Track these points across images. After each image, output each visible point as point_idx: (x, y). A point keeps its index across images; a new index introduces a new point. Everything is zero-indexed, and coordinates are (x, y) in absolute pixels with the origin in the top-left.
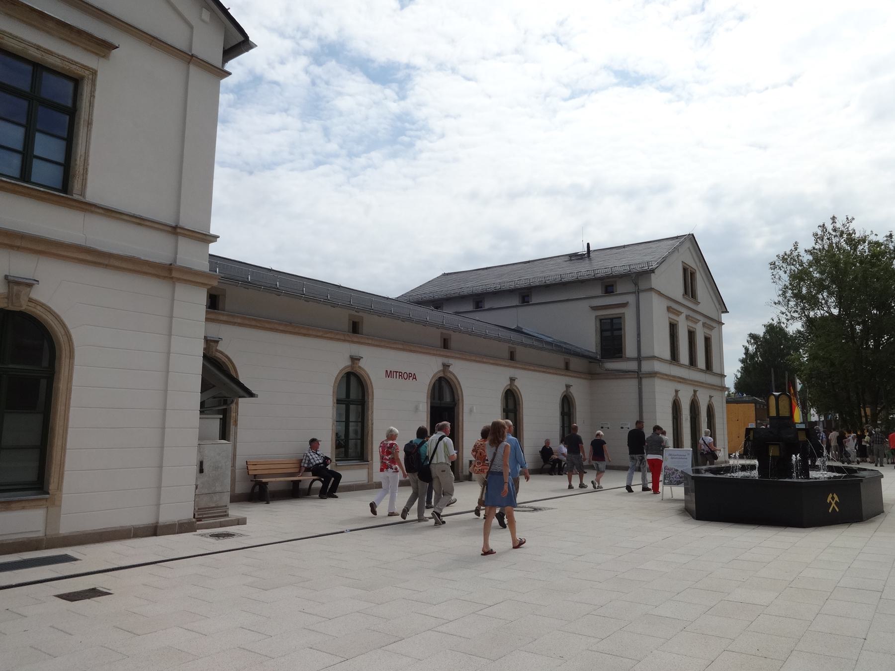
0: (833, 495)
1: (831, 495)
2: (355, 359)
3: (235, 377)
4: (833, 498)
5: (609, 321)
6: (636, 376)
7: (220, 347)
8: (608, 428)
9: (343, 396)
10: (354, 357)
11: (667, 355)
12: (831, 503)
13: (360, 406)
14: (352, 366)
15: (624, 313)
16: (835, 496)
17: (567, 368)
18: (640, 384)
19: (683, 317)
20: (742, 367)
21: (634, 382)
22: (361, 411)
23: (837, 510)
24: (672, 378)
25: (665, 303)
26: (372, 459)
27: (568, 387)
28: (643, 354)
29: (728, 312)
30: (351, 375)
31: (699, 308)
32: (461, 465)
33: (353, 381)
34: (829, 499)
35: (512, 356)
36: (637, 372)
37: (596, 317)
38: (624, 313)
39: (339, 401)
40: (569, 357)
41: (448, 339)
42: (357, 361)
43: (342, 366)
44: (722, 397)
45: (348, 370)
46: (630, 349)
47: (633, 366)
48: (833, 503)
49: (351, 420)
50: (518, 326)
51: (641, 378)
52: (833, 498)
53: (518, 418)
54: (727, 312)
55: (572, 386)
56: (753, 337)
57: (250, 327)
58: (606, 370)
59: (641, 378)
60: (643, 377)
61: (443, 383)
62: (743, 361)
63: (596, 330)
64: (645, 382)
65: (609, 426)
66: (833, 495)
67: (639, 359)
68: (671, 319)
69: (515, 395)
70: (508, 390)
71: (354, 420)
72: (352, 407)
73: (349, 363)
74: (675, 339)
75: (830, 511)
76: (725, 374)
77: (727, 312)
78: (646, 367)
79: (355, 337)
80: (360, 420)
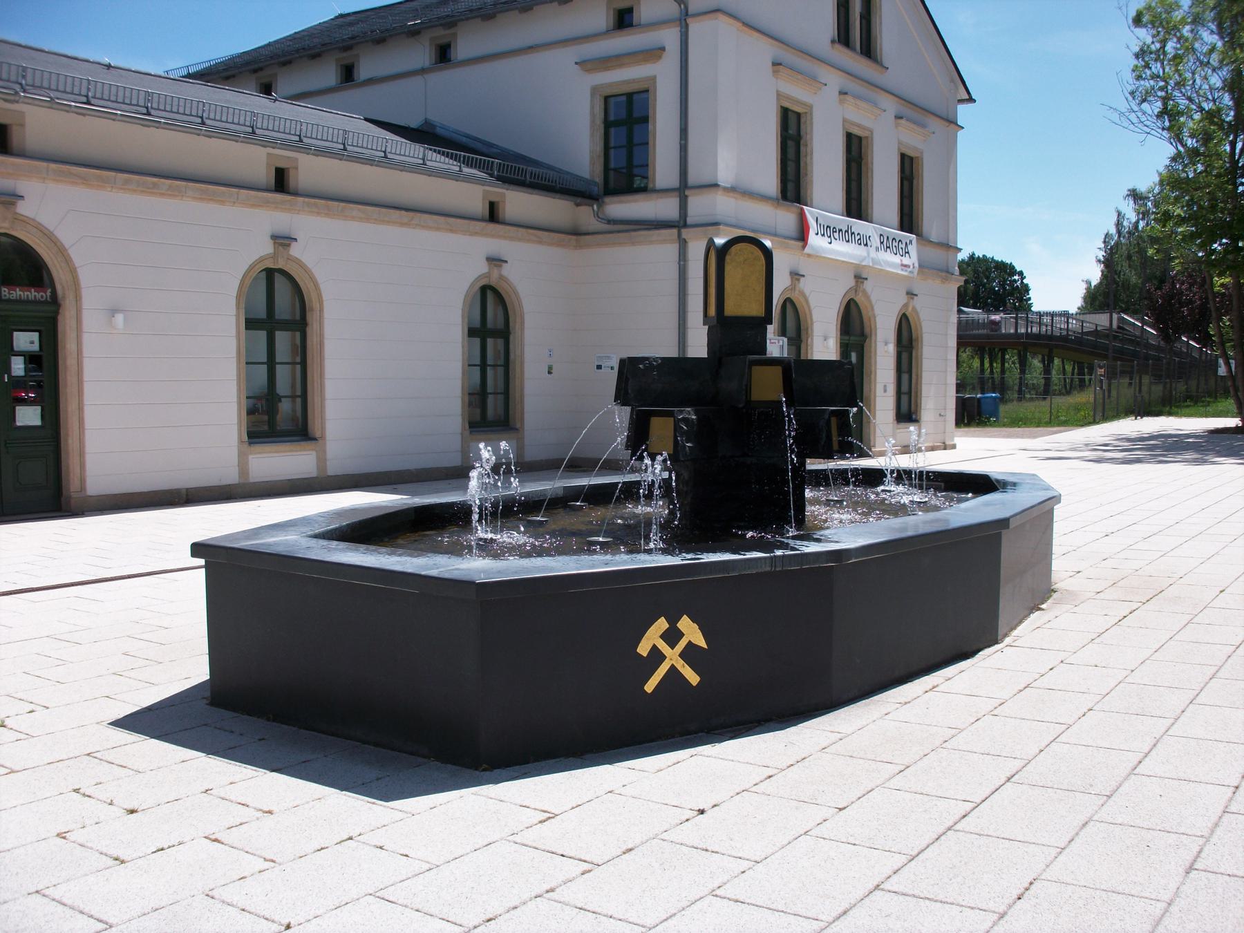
0: (673, 621)
1: (662, 624)
2: (282, 241)
3: (296, 296)
4: (672, 636)
5: (624, 98)
11: (769, 181)
12: (656, 656)
13: (298, 334)
15: (653, 79)
16: (685, 624)
17: (493, 214)
19: (831, 92)
23: (650, 687)
25: (764, 51)
27: (495, 261)
28: (693, 178)
29: (975, 101)
30: (276, 274)
31: (887, 79)
32: (78, 470)
34: (652, 638)
35: (281, 182)
37: (594, 90)
38: (653, 79)
40: (504, 191)
41: (10, 125)
46: (664, 169)
47: (666, 208)
48: (672, 657)
52: (672, 636)
54: (971, 100)
56: (1135, 195)
61: (788, 305)
63: (593, 122)
66: (673, 621)
67: (683, 189)
68: (788, 98)
70: (484, 290)
71: (492, 364)
73: (267, 248)
74: (802, 148)
77: (971, 100)
78: (698, 206)
80: (298, 359)
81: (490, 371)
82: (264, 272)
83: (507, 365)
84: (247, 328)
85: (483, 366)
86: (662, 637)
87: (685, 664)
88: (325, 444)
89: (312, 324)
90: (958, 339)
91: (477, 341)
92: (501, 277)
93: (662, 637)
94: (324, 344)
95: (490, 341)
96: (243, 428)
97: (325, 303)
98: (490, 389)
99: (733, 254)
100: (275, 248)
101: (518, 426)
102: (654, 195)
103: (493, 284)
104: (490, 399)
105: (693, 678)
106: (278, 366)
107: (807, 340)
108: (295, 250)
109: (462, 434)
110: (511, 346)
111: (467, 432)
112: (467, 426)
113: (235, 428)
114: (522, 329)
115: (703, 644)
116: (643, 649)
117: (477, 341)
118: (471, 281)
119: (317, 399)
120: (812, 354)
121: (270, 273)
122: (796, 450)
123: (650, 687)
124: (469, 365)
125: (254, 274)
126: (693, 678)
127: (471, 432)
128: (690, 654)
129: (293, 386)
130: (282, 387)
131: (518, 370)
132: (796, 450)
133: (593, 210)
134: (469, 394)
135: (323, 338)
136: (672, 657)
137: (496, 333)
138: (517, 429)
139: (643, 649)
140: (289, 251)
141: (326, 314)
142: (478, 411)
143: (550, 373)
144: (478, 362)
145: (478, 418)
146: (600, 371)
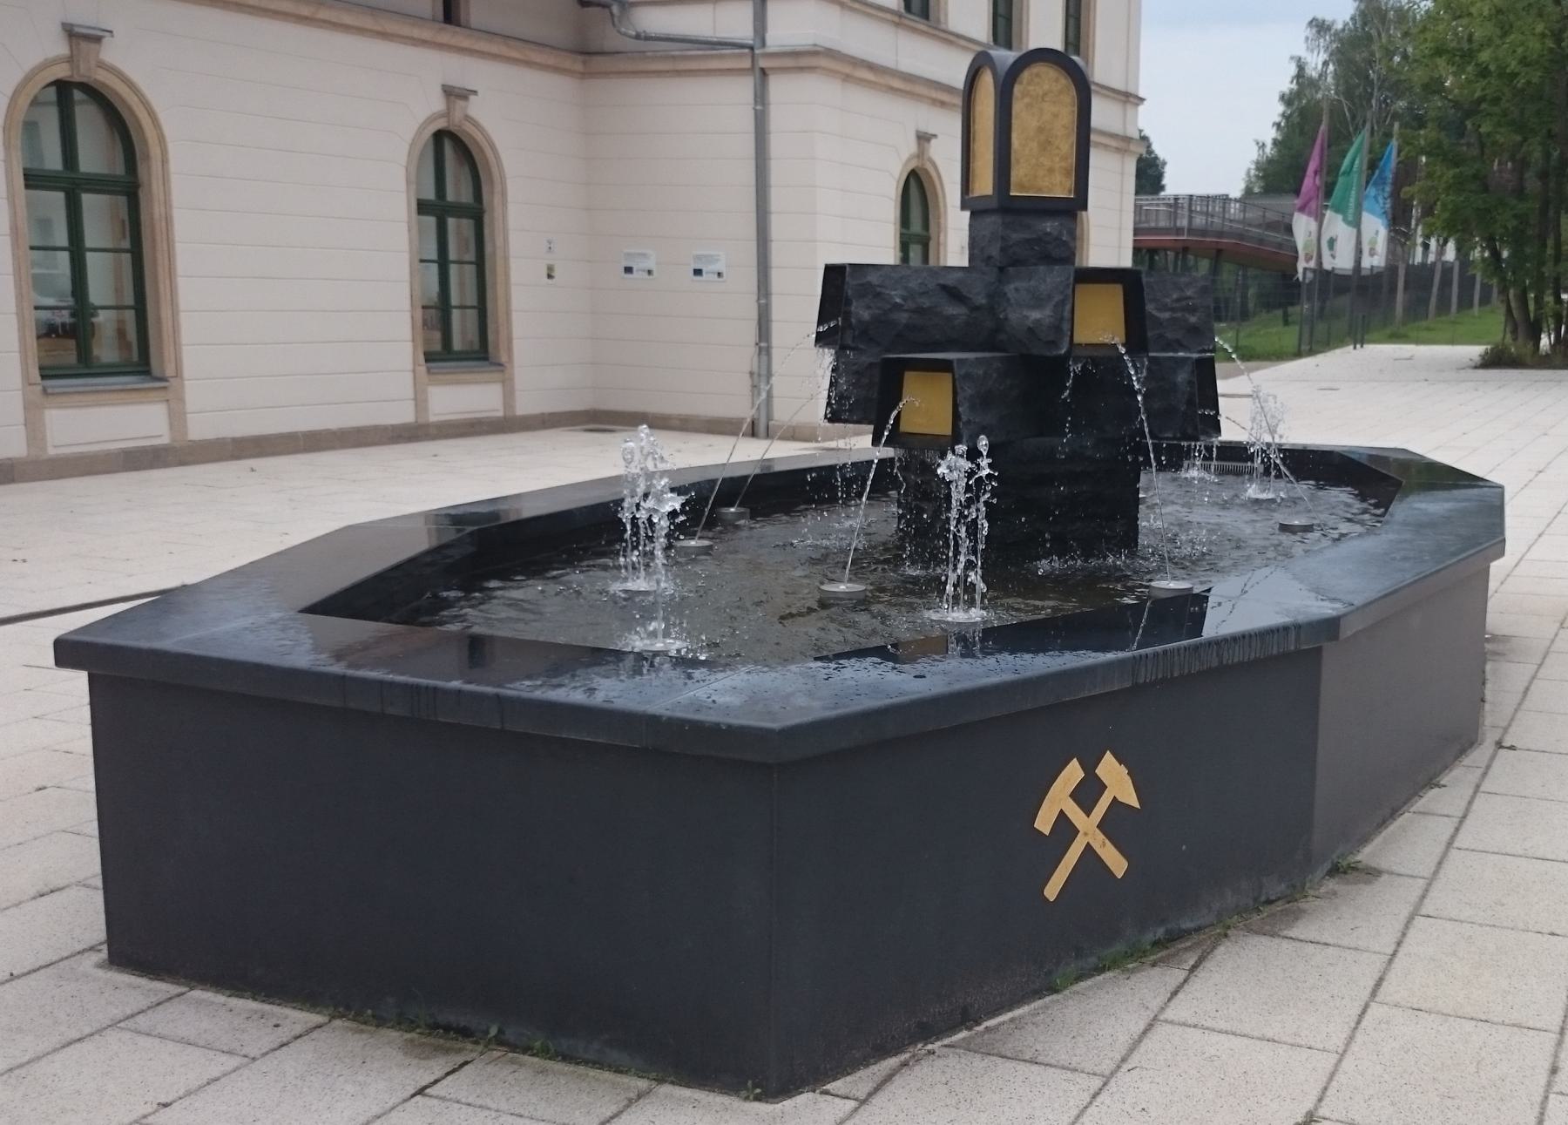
0: (1089, 766)
1: (1073, 773)
6: (747, 64)
7: (110, 53)
8: (650, 272)
9: (430, 195)
10: (77, 30)
14: (447, 114)
16: (1111, 771)
18: (761, 97)
20: (1283, 115)
21: (743, 89)
22: (126, 218)
24: (897, 84)
26: (178, 374)
27: (454, 94)
33: (88, 119)
34: (1059, 799)
36: (752, 48)
39: (423, 207)
42: (93, 46)
43: (422, 113)
44: (1122, 174)
45: (441, 124)
48: (1088, 826)
49: (89, 243)
50: (1125, 110)
51: (764, 72)
52: (1087, 794)
53: (144, 217)
55: (475, 92)
56: (1320, 27)
57: (250, 13)
58: (638, 37)
59: (764, 72)
60: (774, 69)
61: (913, 183)
62: (1287, 100)
64: (779, 87)
65: (651, 264)
66: (1089, 766)
69: (125, 115)
70: (439, 137)
72: (91, 203)
73: (438, 104)
75: (1052, 891)
76: (1141, 95)
79: (449, 35)
81: (453, 270)
82: (53, 90)
83: (480, 263)
84: (27, 186)
85: (443, 262)
86: (1074, 795)
87: (1107, 841)
88: (182, 386)
89: (150, 185)
90: (901, 237)
91: (431, 221)
92: (467, 118)
93: (1074, 795)
94: (171, 217)
95: (451, 222)
96: (30, 362)
97: (170, 146)
98: (455, 300)
99: (1025, 82)
100: (71, 46)
101: (504, 359)
102: (468, 32)
103: (452, 129)
104: (456, 314)
105: (1117, 864)
106: (89, 255)
107: (939, 237)
108: (110, 53)
109: (414, 371)
110: (486, 231)
111: (422, 369)
112: (422, 358)
113: (16, 358)
114: (504, 203)
115: (1134, 802)
116: (1044, 822)
117: (431, 221)
118: (421, 121)
119: (166, 313)
120: (945, 260)
121: (63, 88)
122: (1125, 428)
123: (1052, 891)
124: (422, 261)
125: (34, 89)
126: (1117, 864)
127: (429, 371)
128: (1116, 823)
129: (118, 291)
130: (99, 289)
131: (500, 270)
132: (1125, 428)
133: (612, 14)
134: (424, 307)
135: (171, 206)
136: (1088, 826)
137: (459, 210)
138: (500, 365)
139: (1044, 822)
140: (98, 53)
141: (173, 166)
142: (437, 335)
143: (550, 276)
144: (434, 256)
145: (438, 347)
146: (698, 278)
